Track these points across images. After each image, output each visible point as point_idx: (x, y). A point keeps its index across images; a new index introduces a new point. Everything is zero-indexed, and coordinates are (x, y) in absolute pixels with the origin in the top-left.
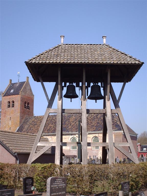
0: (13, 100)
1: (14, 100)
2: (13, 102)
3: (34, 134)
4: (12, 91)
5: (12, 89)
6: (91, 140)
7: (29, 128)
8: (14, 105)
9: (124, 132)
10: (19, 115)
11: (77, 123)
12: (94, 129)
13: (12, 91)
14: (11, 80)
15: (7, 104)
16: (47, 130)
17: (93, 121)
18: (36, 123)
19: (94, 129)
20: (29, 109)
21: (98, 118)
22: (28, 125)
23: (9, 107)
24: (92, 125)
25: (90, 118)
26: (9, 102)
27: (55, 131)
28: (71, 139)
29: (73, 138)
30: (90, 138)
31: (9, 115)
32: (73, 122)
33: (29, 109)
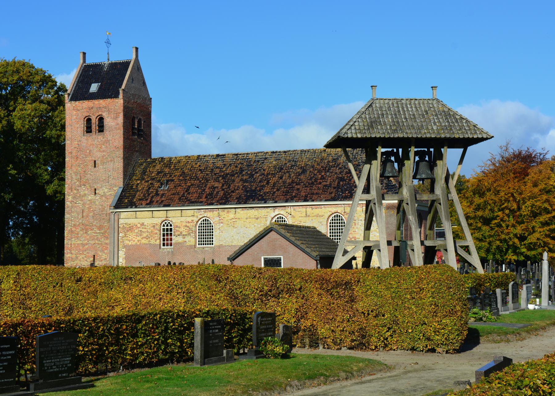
0: (100, 113)
5: (95, 82)
6: (325, 223)
7: (151, 190)
11: (284, 178)
12: (333, 195)
13: (94, 88)
15: (82, 125)
16: (206, 197)
17: (328, 174)
18: (171, 176)
19: (333, 195)
21: (340, 166)
22: (148, 181)
23: (91, 132)
24: (325, 183)
26: (89, 121)
27: (227, 198)
28: (272, 218)
29: (276, 217)
30: (322, 216)
32: (274, 175)
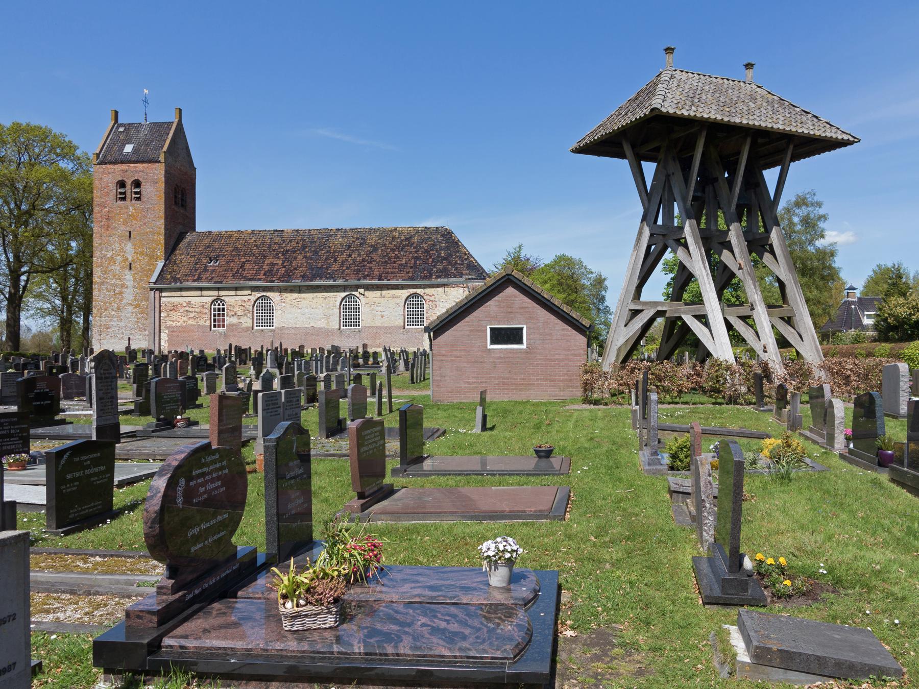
1: (141, 179)
2: (137, 184)
3: (221, 282)
4: (128, 148)
8: (144, 193)
9: (15, 304)
10: (163, 227)
13: (128, 148)
14: (116, 113)
20: (186, 209)
25: (390, 243)
31: (125, 223)
32: (342, 253)
33: (186, 209)
